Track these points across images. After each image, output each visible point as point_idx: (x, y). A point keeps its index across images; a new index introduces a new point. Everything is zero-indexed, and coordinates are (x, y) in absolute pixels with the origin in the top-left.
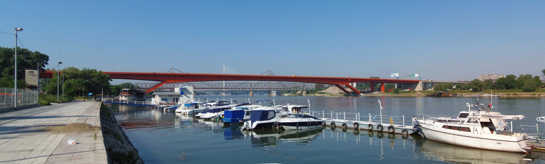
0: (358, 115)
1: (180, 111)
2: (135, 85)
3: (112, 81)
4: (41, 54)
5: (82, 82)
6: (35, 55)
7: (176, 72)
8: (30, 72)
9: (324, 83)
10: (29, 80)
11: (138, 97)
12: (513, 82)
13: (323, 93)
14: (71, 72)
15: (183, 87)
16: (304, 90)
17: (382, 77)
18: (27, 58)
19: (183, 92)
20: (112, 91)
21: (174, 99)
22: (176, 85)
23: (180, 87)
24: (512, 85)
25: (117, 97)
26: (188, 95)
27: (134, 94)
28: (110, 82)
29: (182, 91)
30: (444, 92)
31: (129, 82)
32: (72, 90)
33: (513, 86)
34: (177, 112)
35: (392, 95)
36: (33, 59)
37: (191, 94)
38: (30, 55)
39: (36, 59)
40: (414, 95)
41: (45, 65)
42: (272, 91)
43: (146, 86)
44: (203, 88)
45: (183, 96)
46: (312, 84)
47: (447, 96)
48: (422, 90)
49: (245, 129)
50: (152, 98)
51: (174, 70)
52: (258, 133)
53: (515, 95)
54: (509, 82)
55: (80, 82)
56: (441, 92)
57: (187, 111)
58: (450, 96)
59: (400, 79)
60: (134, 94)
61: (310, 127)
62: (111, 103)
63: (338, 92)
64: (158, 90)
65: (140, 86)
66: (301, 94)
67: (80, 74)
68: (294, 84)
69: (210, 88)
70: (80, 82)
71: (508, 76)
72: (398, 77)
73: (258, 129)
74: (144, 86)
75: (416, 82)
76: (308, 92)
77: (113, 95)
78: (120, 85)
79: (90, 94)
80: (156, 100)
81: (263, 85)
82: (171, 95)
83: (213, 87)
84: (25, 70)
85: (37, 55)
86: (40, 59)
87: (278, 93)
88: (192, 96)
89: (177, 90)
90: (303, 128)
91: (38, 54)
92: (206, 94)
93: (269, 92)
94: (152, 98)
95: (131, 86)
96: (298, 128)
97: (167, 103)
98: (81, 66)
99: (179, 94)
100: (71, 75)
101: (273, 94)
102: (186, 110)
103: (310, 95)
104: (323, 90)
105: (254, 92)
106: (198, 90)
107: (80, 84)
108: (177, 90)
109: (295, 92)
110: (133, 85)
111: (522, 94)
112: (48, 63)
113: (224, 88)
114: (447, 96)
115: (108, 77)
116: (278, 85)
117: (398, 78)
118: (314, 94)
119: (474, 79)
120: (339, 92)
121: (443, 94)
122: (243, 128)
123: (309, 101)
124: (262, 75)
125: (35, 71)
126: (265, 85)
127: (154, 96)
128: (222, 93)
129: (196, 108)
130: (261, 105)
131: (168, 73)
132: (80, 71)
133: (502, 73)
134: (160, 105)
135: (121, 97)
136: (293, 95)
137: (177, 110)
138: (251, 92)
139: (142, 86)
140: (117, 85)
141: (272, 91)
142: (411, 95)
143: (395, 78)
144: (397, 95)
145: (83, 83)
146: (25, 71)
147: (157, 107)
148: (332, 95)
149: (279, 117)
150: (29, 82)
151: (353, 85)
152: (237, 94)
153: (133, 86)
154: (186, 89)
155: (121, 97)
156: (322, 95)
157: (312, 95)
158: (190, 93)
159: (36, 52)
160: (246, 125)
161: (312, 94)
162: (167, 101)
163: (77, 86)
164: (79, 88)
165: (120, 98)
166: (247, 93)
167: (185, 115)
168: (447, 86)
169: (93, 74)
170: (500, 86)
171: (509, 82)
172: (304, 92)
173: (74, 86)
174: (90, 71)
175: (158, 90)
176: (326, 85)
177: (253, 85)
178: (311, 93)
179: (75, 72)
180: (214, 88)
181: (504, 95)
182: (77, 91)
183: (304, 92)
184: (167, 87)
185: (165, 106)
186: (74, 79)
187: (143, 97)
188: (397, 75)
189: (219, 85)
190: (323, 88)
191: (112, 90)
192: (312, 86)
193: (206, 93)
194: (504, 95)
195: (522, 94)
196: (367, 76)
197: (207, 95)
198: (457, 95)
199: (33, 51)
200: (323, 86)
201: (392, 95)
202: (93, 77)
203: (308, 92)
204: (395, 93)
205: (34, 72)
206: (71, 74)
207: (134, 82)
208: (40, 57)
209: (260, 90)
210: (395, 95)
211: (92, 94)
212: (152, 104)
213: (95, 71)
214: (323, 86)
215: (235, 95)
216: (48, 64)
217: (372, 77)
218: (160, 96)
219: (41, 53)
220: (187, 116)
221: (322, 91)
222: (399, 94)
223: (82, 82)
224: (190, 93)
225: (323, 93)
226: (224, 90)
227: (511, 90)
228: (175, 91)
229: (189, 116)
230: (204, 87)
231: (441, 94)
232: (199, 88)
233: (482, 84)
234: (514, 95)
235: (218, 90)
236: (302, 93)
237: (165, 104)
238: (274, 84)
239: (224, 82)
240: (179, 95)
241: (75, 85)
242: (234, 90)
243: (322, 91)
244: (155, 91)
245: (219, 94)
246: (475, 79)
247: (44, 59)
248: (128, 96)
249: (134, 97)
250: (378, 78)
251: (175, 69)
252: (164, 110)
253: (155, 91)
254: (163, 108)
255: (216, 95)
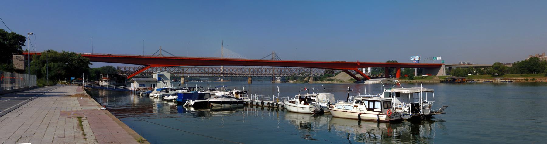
0: (338, 101)
1: (153, 95)
2: (117, 68)
3: (92, 64)
4: (18, 35)
5: (62, 66)
6: (12, 36)
7: (166, 55)
8: (17, 57)
9: (334, 69)
10: (16, 65)
11: (118, 82)
12: (536, 65)
13: (332, 80)
14: (51, 56)
15: (160, 73)
16: (311, 76)
17: (400, 61)
18: (4, 40)
19: (161, 78)
20: (91, 75)
21: (152, 84)
22: (154, 69)
23: (157, 73)
24: (534, 68)
25: (97, 82)
26: (165, 81)
27: (114, 79)
28: (90, 66)
29: (159, 77)
30: (457, 77)
31: (108, 65)
32: (53, 73)
33: (536, 70)
34: (150, 96)
35: (405, 81)
36: (10, 40)
37: (168, 80)
38: (7, 36)
39: (13, 41)
40: (429, 82)
41: (22, 46)
42: (277, 77)
43: (130, 69)
44: (194, 73)
45: (160, 81)
46: (321, 70)
47: (461, 82)
48: (445, 75)
49: (186, 106)
50: (131, 83)
51: (162, 51)
52: (195, 109)
53: (533, 79)
54: (532, 66)
55: (60, 66)
56: (455, 77)
57: (158, 95)
58: (465, 82)
59: (421, 63)
60: (114, 79)
61: (232, 105)
62: (91, 87)
63: (349, 78)
64: (143, 75)
65: (122, 69)
66: (307, 82)
67: (59, 57)
68: (233, 69)
69: (202, 73)
70: (60, 66)
71: (531, 59)
72: (419, 61)
73: (196, 106)
74: (127, 70)
75: (438, 67)
76: (315, 79)
77: (93, 80)
78: (100, 68)
79: (72, 78)
80: (134, 86)
81: (264, 70)
82: (149, 81)
83: (205, 72)
84: (13, 55)
85: (14, 36)
86: (17, 41)
87: (284, 80)
88: (169, 82)
89: (155, 76)
90: (226, 105)
91: (14, 35)
92: (200, 80)
93: (273, 79)
94: (131, 83)
95: (112, 70)
96: (221, 105)
97: (144, 88)
98: (60, 49)
99: (156, 80)
100: (50, 59)
101: (278, 80)
102: (157, 94)
103: (317, 82)
104: (334, 76)
105: (254, 79)
106: (189, 75)
107: (60, 68)
108: (155, 76)
109: (302, 78)
110: (115, 68)
111: (541, 79)
112: (25, 44)
113: (222, 74)
114: (461, 82)
115: (87, 60)
116: (281, 71)
117: (419, 62)
118: (322, 80)
119: (495, 63)
120: (350, 79)
121: (456, 79)
122: (185, 104)
123: (314, 90)
124: (263, 60)
125: (22, 56)
126: (266, 70)
127: (133, 82)
128: (220, 79)
129: (166, 92)
130: (218, 90)
131: (153, 56)
132: (59, 54)
133: (523, 56)
134: (138, 90)
135: (101, 82)
136: (299, 82)
137: (150, 95)
138: (249, 79)
139: (125, 69)
140: (97, 69)
141: (277, 77)
142: (425, 82)
143: (415, 62)
144: (411, 81)
145: (64, 67)
146: (13, 56)
147: (135, 92)
148: (341, 82)
149: (213, 97)
150: (16, 66)
151: (367, 71)
152: (238, 81)
153: (114, 69)
154: (163, 75)
155: (102, 82)
156: (330, 82)
157: (320, 82)
158: (167, 79)
159: (13, 33)
160: (188, 103)
161: (320, 80)
162: (145, 86)
163: (57, 70)
164: (59, 72)
165: (100, 83)
166: (245, 79)
167: (157, 98)
168: (466, 71)
169: (72, 58)
170: (522, 70)
171: (532, 66)
172: (311, 79)
173: (54, 70)
174: (69, 55)
175: (143, 75)
176: (337, 71)
177: (252, 70)
178: (319, 80)
179: (54, 56)
180: (211, 74)
181: (522, 80)
182: (57, 74)
183: (311, 79)
184: (218, 72)
185: (142, 91)
186: (53, 62)
187: (124, 82)
188: (417, 58)
189: (217, 70)
190: (333, 74)
191: (91, 74)
192: (321, 72)
193: (201, 78)
194: (522, 80)
195: (541, 79)
196: (384, 61)
197: (202, 81)
198: (474, 80)
199: (10, 32)
200: (334, 72)
201: (405, 81)
202: (73, 60)
203: (315, 79)
204: (409, 79)
205: (20, 57)
206: (50, 57)
207: (115, 65)
208: (16, 38)
209: (259, 76)
210: (409, 81)
211: (74, 78)
212: (131, 89)
213: (75, 54)
214: (334, 72)
215: (236, 81)
216: (25, 46)
217: (389, 61)
218: (138, 81)
219: (17, 33)
220: (158, 99)
221: (332, 78)
222: (413, 80)
223: (62, 66)
224: (167, 79)
225: (332, 80)
226: (222, 75)
227: (534, 74)
228: (153, 77)
229: (159, 99)
230: (195, 72)
231: (454, 79)
232: (189, 73)
233: (503, 68)
234: (533, 80)
235: (216, 75)
236: (309, 79)
237: (143, 90)
238: (278, 69)
239: (222, 67)
240: (156, 81)
241: (55, 69)
242: (234, 75)
243: (332, 78)
244: (140, 75)
245: (216, 80)
246: (496, 63)
247: (21, 41)
248: (108, 80)
249: (114, 82)
250: (396, 62)
251: (163, 50)
252: (141, 94)
253: (140, 75)
254: (139, 93)
255: (213, 81)
